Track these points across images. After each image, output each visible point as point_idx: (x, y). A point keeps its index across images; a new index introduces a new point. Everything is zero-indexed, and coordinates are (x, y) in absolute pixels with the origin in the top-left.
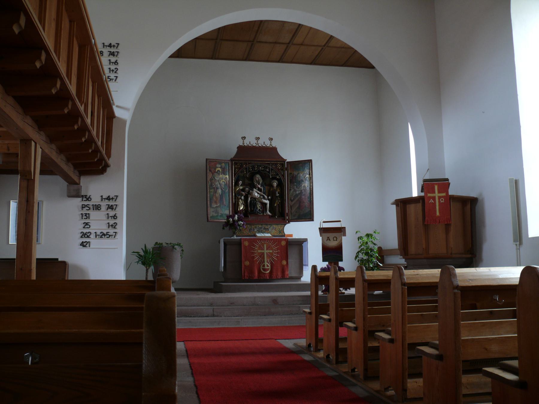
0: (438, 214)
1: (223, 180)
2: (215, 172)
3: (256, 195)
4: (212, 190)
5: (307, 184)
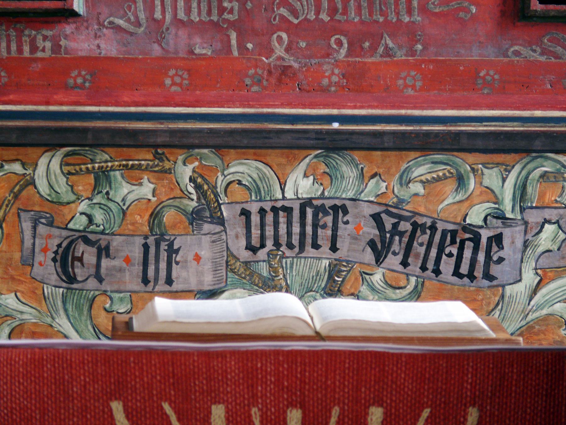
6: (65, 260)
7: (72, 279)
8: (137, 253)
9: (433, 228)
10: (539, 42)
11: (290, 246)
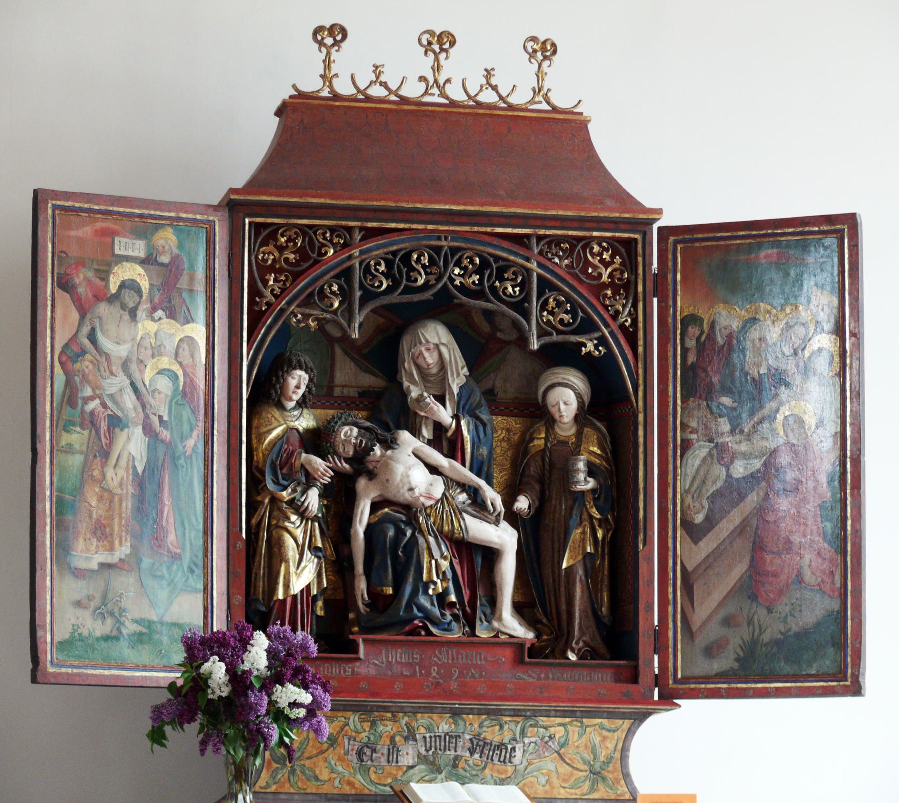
1: (166, 362)
2: (101, 296)
4: (77, 438)
5: (808, 406)
6: (360, 753)
7: (362, 761)
8: (386, 752)
9: (491, 744)
10: (527, 672)
11: (440, 750)
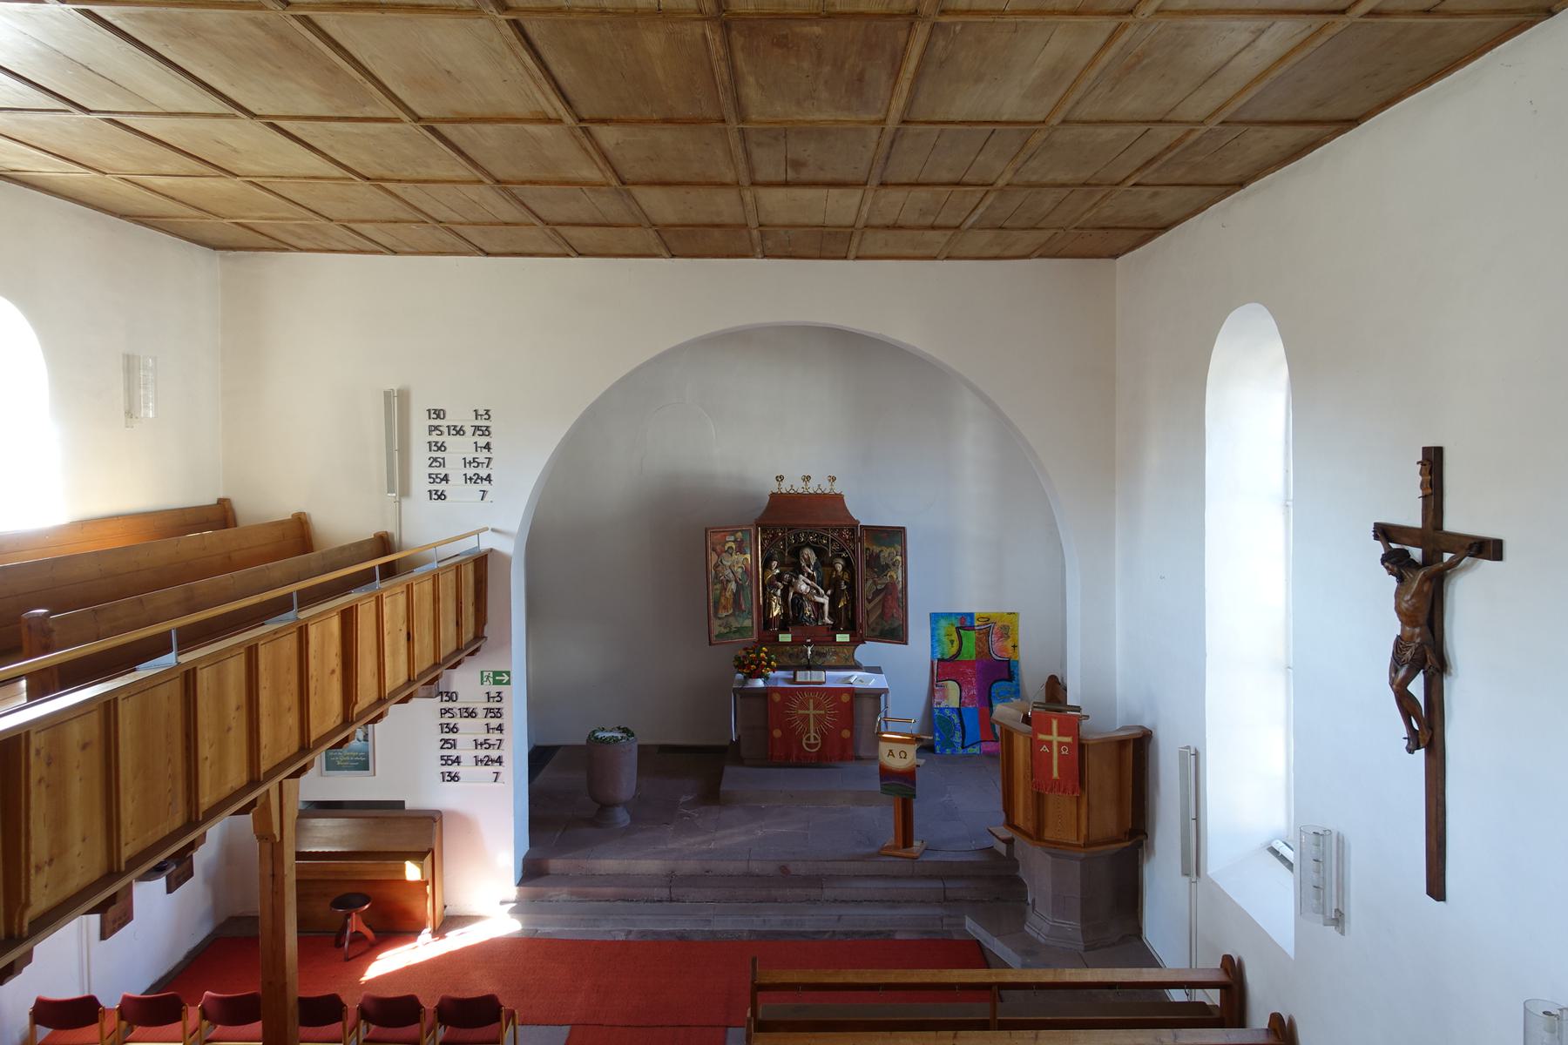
0: (1055, 774)
3: (803, 587)
